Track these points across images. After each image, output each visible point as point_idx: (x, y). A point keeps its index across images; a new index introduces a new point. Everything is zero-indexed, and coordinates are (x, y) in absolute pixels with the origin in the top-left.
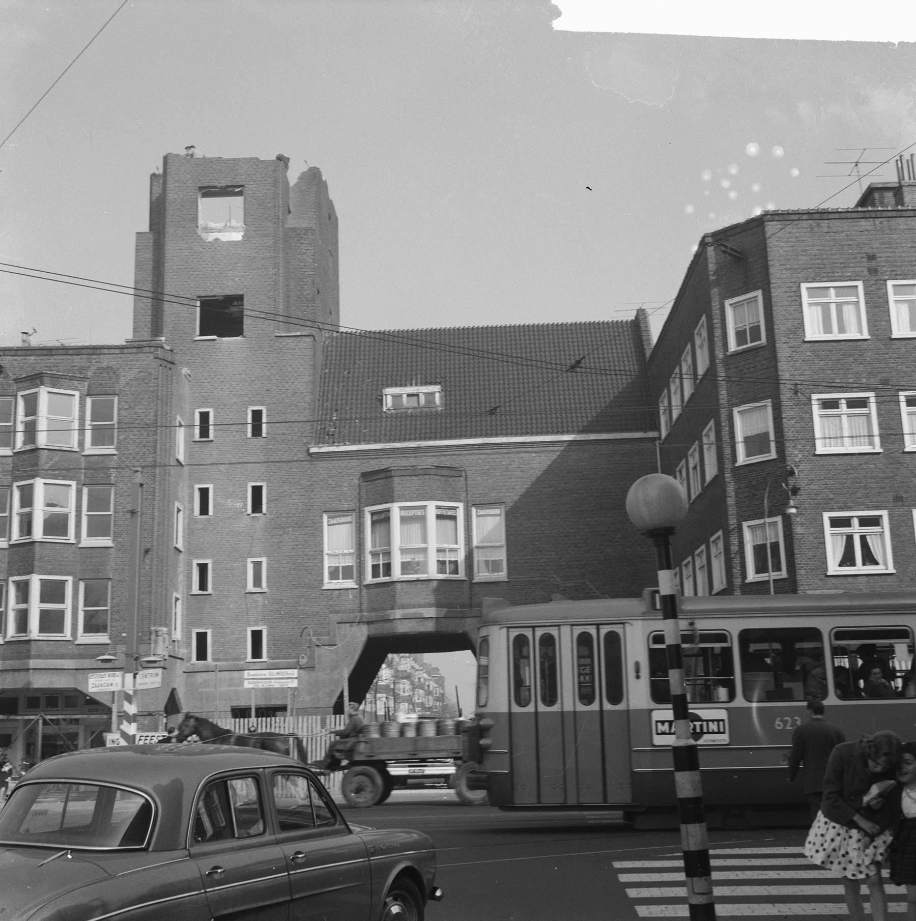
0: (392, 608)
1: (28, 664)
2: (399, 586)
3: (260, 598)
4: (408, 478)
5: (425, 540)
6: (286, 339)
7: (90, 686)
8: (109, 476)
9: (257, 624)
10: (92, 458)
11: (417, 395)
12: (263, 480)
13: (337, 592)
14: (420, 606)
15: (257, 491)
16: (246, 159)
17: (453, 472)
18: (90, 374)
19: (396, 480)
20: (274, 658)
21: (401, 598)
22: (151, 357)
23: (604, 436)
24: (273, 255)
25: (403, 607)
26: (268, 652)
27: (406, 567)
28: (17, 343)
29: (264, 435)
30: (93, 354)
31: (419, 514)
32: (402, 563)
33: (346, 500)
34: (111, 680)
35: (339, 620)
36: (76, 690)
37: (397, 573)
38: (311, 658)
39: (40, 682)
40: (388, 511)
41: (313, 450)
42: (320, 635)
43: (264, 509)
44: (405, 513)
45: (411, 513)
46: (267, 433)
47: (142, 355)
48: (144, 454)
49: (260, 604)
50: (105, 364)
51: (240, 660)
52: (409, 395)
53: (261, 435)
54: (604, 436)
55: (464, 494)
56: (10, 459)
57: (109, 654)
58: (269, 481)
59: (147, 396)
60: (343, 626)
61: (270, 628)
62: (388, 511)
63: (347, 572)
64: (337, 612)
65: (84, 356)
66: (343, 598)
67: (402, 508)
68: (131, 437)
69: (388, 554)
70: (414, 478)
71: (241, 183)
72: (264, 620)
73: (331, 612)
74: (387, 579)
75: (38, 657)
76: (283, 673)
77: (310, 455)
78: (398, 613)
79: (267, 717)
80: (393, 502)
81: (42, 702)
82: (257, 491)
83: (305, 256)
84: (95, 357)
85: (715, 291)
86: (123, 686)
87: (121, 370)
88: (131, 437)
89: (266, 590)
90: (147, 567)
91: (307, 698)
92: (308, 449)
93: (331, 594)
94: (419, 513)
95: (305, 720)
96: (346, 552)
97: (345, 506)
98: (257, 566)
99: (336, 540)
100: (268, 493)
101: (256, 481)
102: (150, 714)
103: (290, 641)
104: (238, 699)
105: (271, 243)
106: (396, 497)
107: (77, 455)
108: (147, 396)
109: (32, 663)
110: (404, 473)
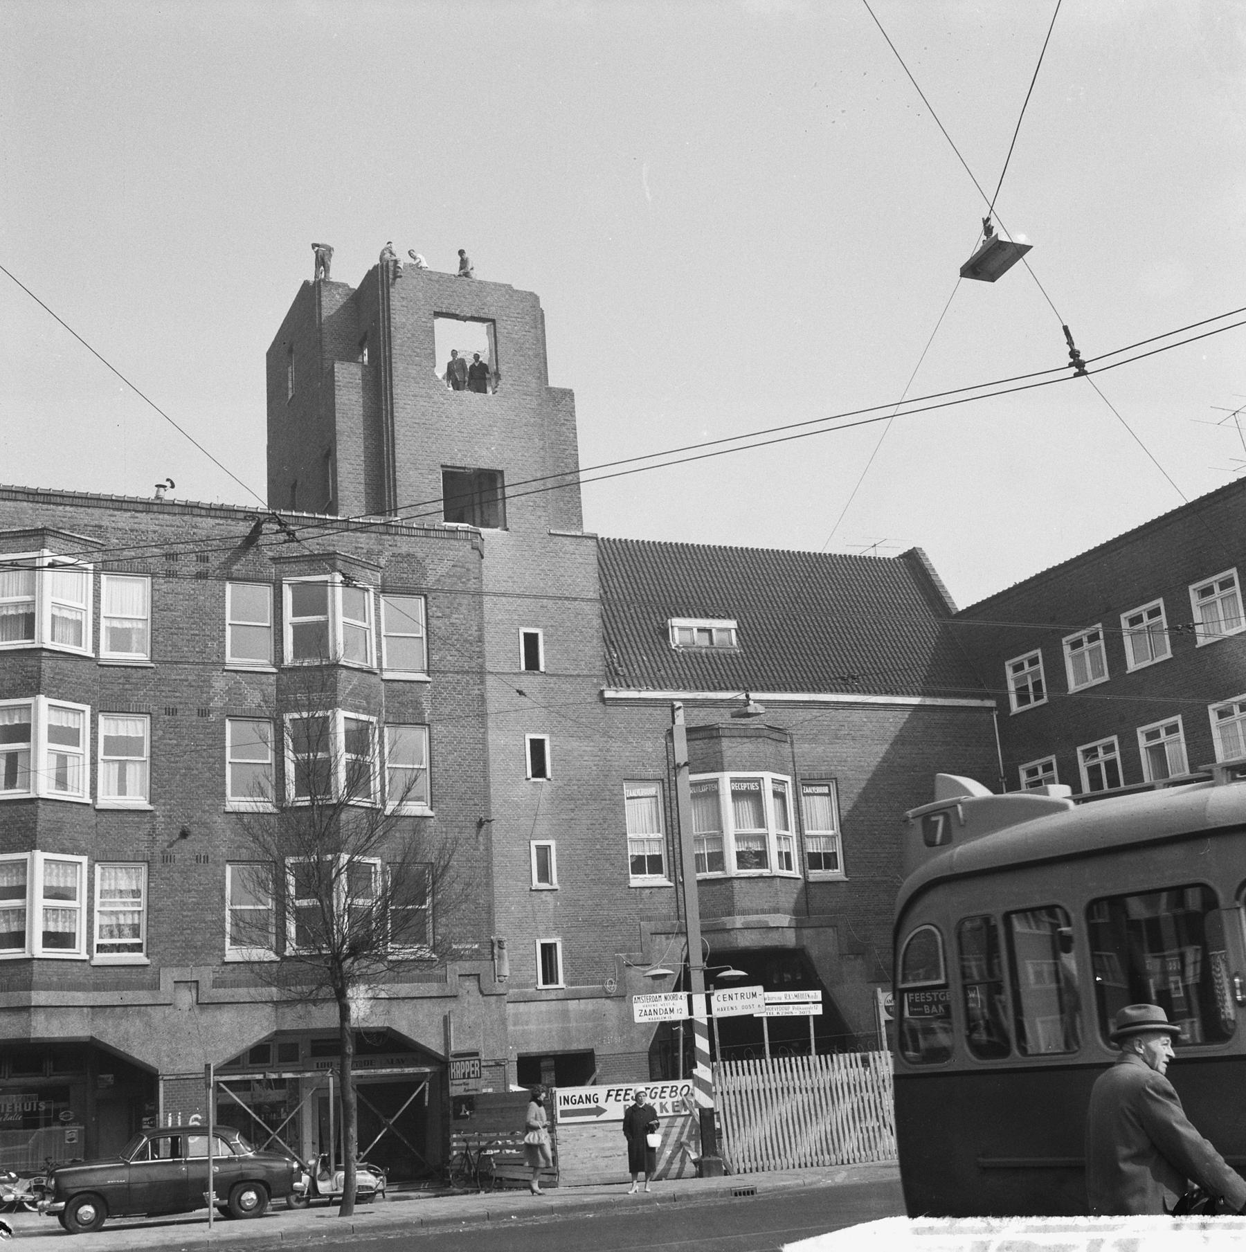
0: (730, 914)
1: (29, 998)
3: (548, 897)
5: (761, 822)
7: (636, 1014)
10: (395, 684)
11: (709, 631)
13: (647, 891)
14: (764, 912)
16: (495, 284)
17: (778, 734)
18: (383, 562)
19: (725, 743)
20: (572, 984)
21: (741, 901)
22: (469, 547)
24: (539, 421)
25: (744, 912)
26: (565, 974)
27: (742, 859)
28: (149, 493)
29: (542, 668)
32: (738, 853)
33: (651, 766)
34: (670, 1004)
36: (388, 1028)
38: (622, 982)
39: (45, 1028)
42: (630, 950)
43: (549, 774)
45: (744, 787)
46: (546, 667)
47: (455, 543)
48: (468, 683)
49: (551, 906)
51: (527, 986)
52: (699, 630)
53: (538, 669)
55: (791, 765)
56: (273, 678)
59: (465, 602)
60: (658, 938)
61: (566, 940)
62: (716, 781)
63: (654, 864)
64: (649, 919)
65: (373, 535)
67: (733, 780)
68: (449, 658)
71: (490, 317)
72: (557, 929)
73: (642, 919)
74: (717, 874)
75: (47, 987)
77: (604, 700)
78: (739, 921)
80: (722, 770)
83: (564, 429)
84: (387, 537)
86: (691, 1013)
88: (449, 658)
89: (556, 886)
91: (617, 1040)
92: (602, 692)
93: (641, 894)
95: (841, 1059)
97: (651, 773)
98: (543, 851)
100: (552, 750)
101: (535, 732)
104: (528, 1043)
105: (534, 404)
106: (726, 764)
107: (374, 679)
108: (465, 602)
109: (39, 997)
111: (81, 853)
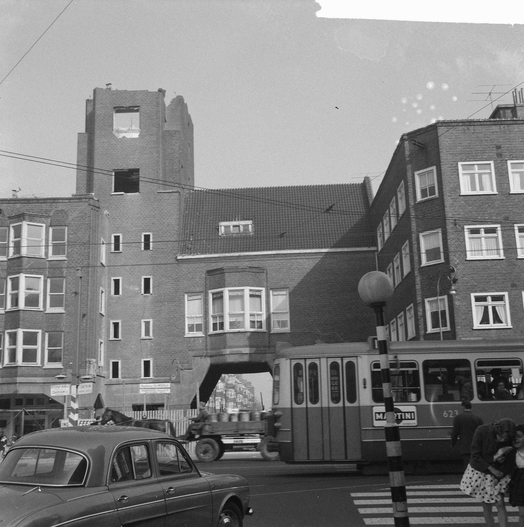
0: (225, 348)
1: (16, 380)
2: (228, 335)
3: (149, 342)
4: (234, 273)
5: (243, 309)
6: (164, 194)
7: (52, 392)
8: (62, 273)
9: (147, 357)
10: (53, 262)
11: (239, 226)
12: (150, 275)
13: (193, 339)
14: (240, 347)
15: (147, 281)
16: (140, 91)
17: (259, 270)
18: (51, 214)
19: (227, 275)
20: (157, 377)
21: (230, 342)
22: (87, 204)
23: (346, 250)
24: (156, 146)
25: (231, 347)
26: (153, 373)
27: (232, 324)
28: (10, 196)
29: (151, 249)
30: (53, 203)
31: (240, 294)
32: (230, 322)
33: (198, 286)
34: (63, 389)
35: (194, 355)
36: (43, 395)
37: (227, 328)
38: (178, 376)
39: (23, 390)
40: (222, 292)
41: (179, 257)
42: (183, 363)
43: (151, 291)
44: (232, 294)
45: (235, 293)
46: (153, 248)
47: (81, 203)
48: (83, 260)
49: (149, 346)
50: (60, 209)
51: (137, 377)
52: (234, 226)
53: (149, 249)
54: (346, 250)
55: (266, 283)
56: (6, 263)
57: (63, 374)
58: (154, 275)
59: (84, 227)
60: (196, 358)
61: (155, 359)
62: (222, 292)
63: (199, 328)
64: (193, 350)
65: (48, 204)
66: (196, 342)
67: (230, 291)
68: (75, 250)
69: (222, 317)
70: (237, 273)
71: (138, 105)
72: (151, 355)
73: (189, 350)
74: (221, 331)
75: (22, 376)
76: (162, 385)
77: (178, 260)
78: (228, 351)
79: (153, 410)
80: (225, 287)
81: (24, 402)
82: (147, 281)
83: (174, 147)
84: (54, 204)
85: (409, 167)
86: (70, 393)
87: (69, 212)
88: (75, 250)
89: (152, 338)
90: (84, 325)
91: (176, 400)
92: (176, 257)
93: (189, 340)
94: (240, 293)
95: (175, 412)
96: (198, 316)
97: (198, 290)
98: (147, 324)
99: (192, 309)
100: (153, 282)
101: (146, 275)
102: (86, 409)
103: (166, 367)
104: (136, 400)
105: (155, 139)
106: (226, 284)
107: (44, 261)
108: (84, 227)
109: (19, 379)
110: (231, 271)
111: (39, 329)
